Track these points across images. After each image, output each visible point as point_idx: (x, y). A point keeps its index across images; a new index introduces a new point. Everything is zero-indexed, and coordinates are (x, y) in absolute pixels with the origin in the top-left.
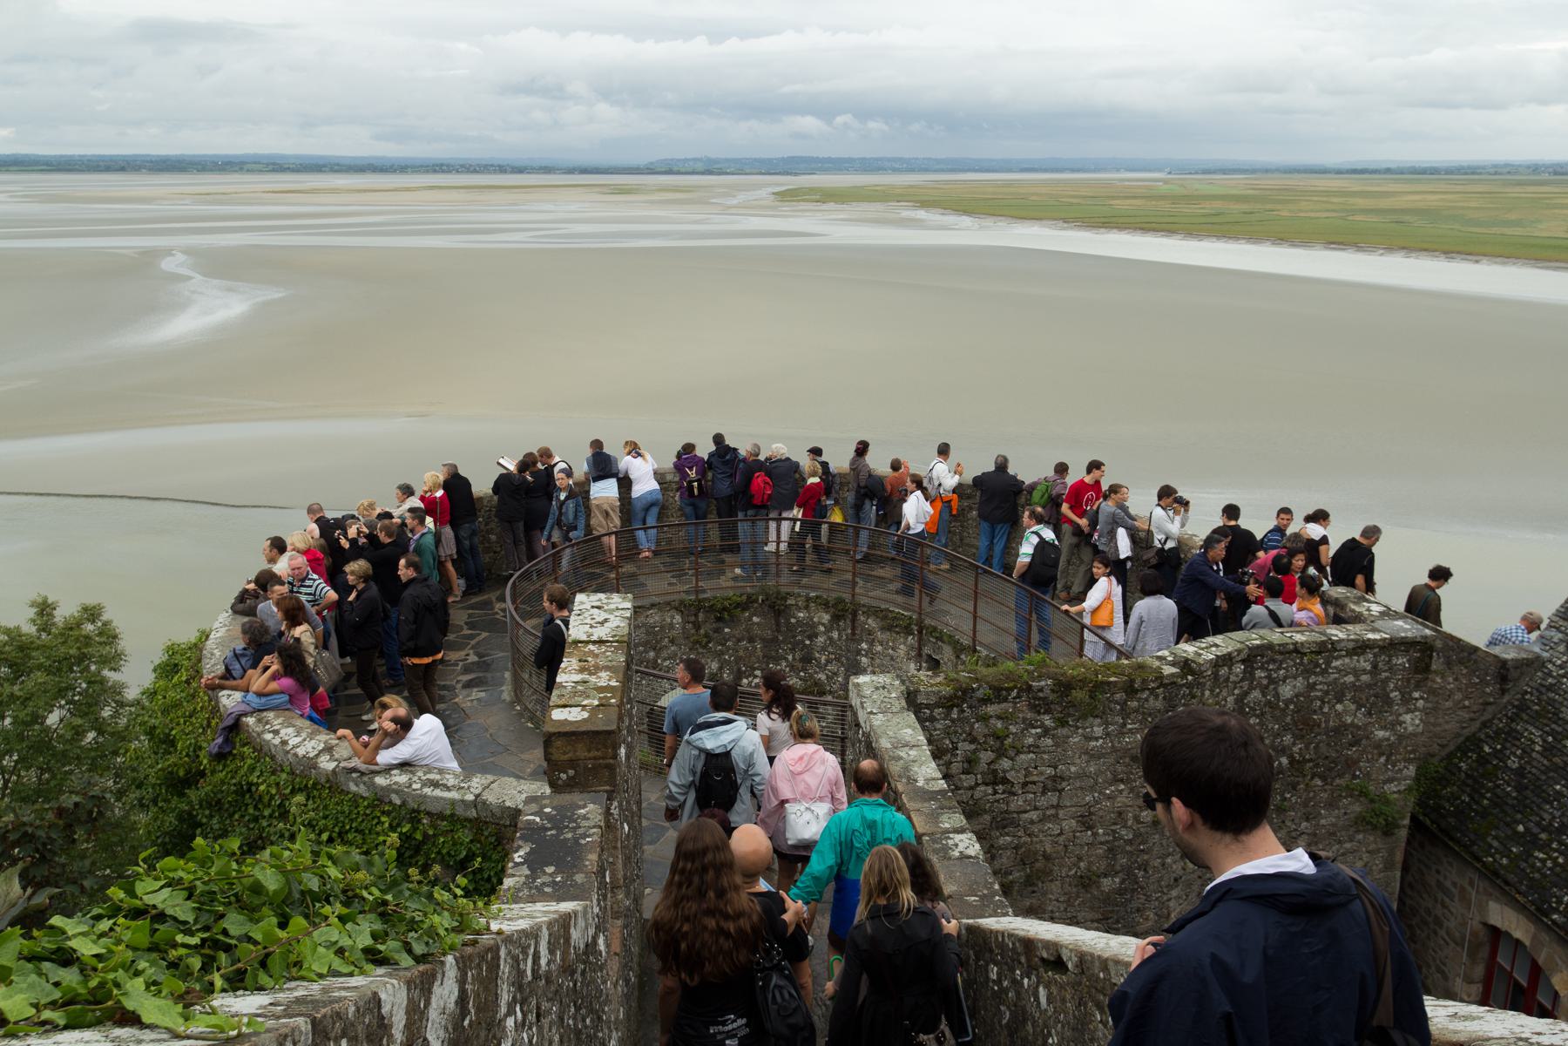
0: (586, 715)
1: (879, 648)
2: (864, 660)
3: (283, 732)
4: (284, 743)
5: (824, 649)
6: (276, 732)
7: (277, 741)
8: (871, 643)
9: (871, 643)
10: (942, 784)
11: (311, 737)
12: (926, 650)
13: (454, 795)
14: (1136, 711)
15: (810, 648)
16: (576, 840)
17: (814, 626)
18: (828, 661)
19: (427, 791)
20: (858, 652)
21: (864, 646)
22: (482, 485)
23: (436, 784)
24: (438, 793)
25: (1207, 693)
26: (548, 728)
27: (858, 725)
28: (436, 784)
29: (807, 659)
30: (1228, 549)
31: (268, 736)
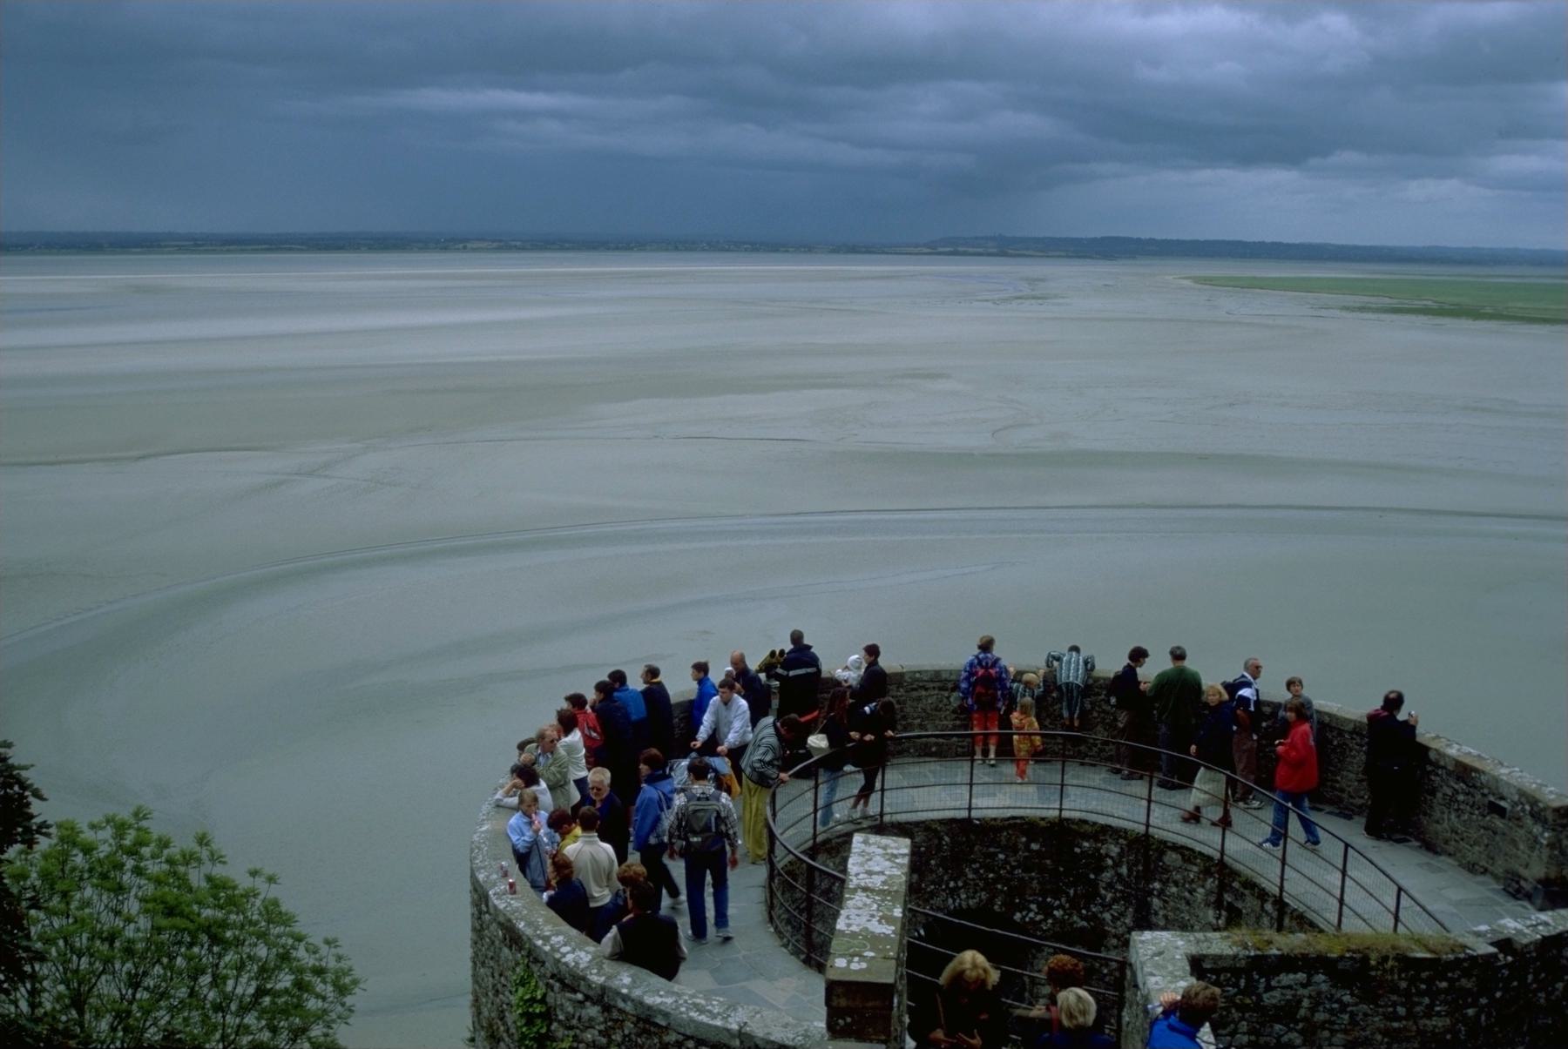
0: (864, 965)
1: (1174, 890)
2: (1155, 901)
3: (554, 940)
4: (554, 949)
5: (1110, 886)
6: (546, 939)
7: (547, 948)
8: (1165, 883)
9: (1165, 883)
10: (269, 986)
11: (580, 947)
12: (1228, 897)
13: (718, 1023)
14: (1446, 991)
15: (1094, 885)
16: (1430, 773)
17: (1102, 858)
18: (1115, 900)
19: (693, 1014)
20: (1150, 893)
21: (1157, 885)
22: (753, 664)
23: (701, 1010)
24: (703, 1018)
25: (1530, 977)
26: (832, 975)
27: (1136, 986)
28: (701, 1010)
29: (1092, 895)
30: (913, 1037)
31: (540, 943)
